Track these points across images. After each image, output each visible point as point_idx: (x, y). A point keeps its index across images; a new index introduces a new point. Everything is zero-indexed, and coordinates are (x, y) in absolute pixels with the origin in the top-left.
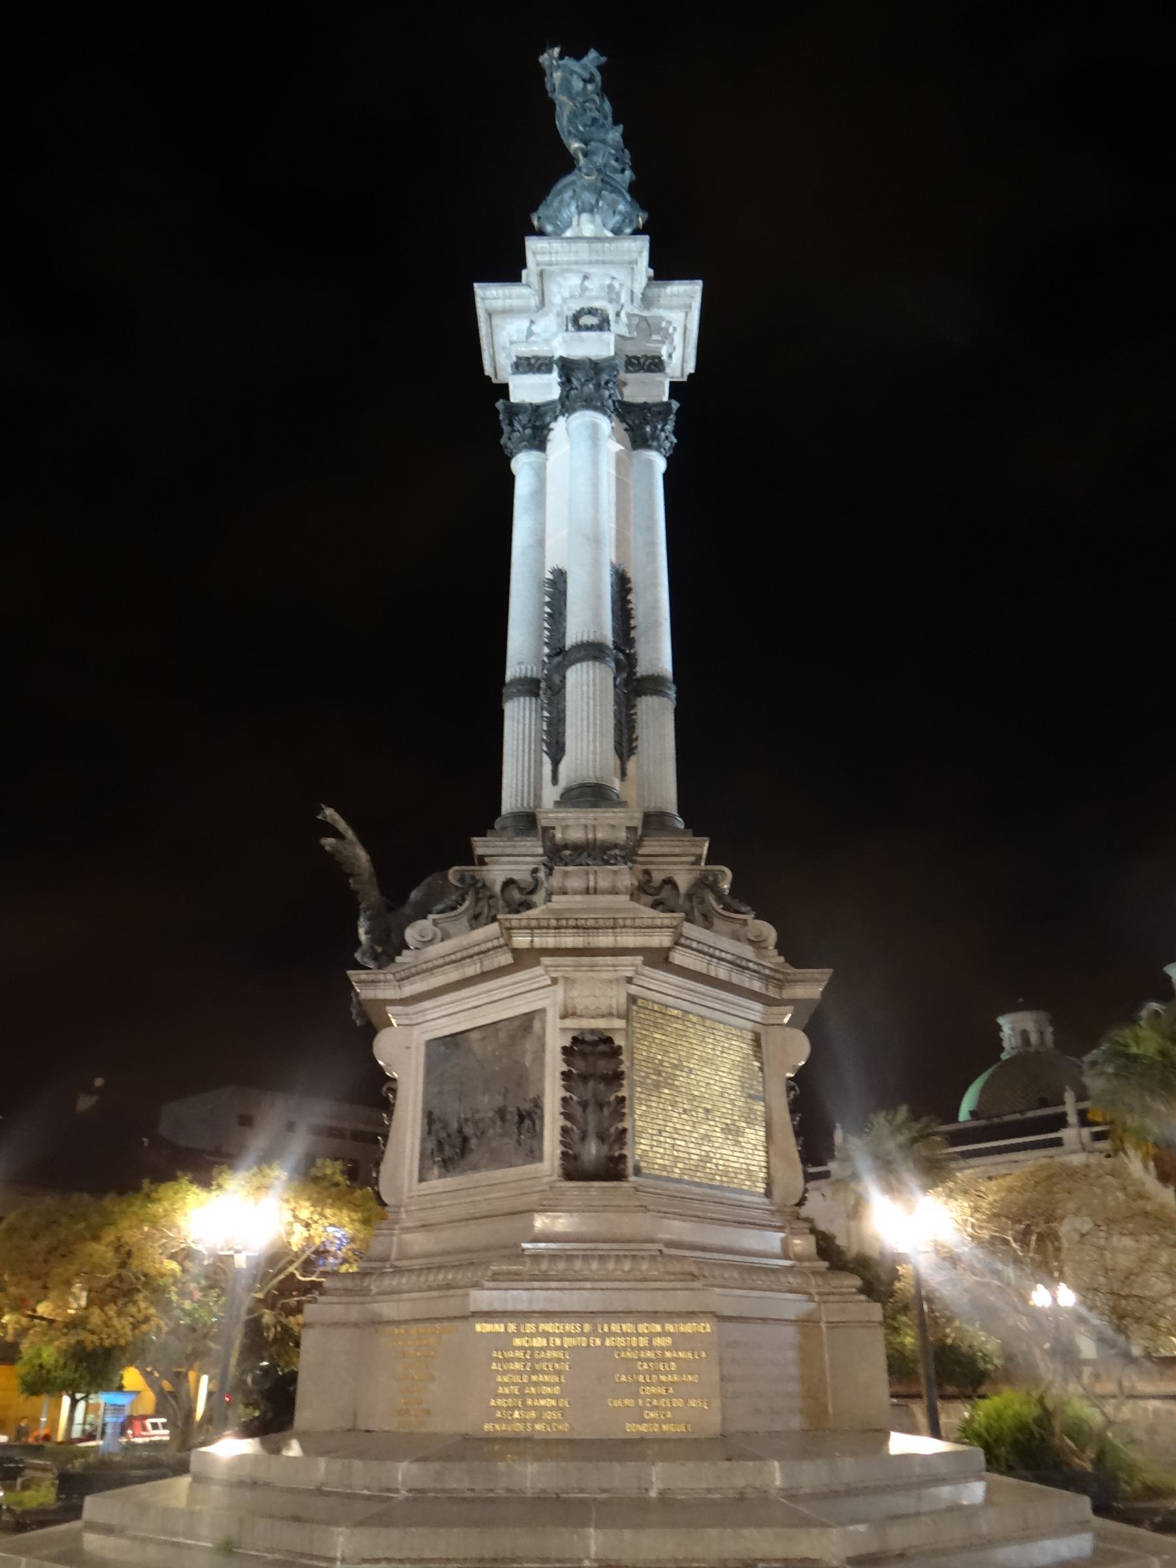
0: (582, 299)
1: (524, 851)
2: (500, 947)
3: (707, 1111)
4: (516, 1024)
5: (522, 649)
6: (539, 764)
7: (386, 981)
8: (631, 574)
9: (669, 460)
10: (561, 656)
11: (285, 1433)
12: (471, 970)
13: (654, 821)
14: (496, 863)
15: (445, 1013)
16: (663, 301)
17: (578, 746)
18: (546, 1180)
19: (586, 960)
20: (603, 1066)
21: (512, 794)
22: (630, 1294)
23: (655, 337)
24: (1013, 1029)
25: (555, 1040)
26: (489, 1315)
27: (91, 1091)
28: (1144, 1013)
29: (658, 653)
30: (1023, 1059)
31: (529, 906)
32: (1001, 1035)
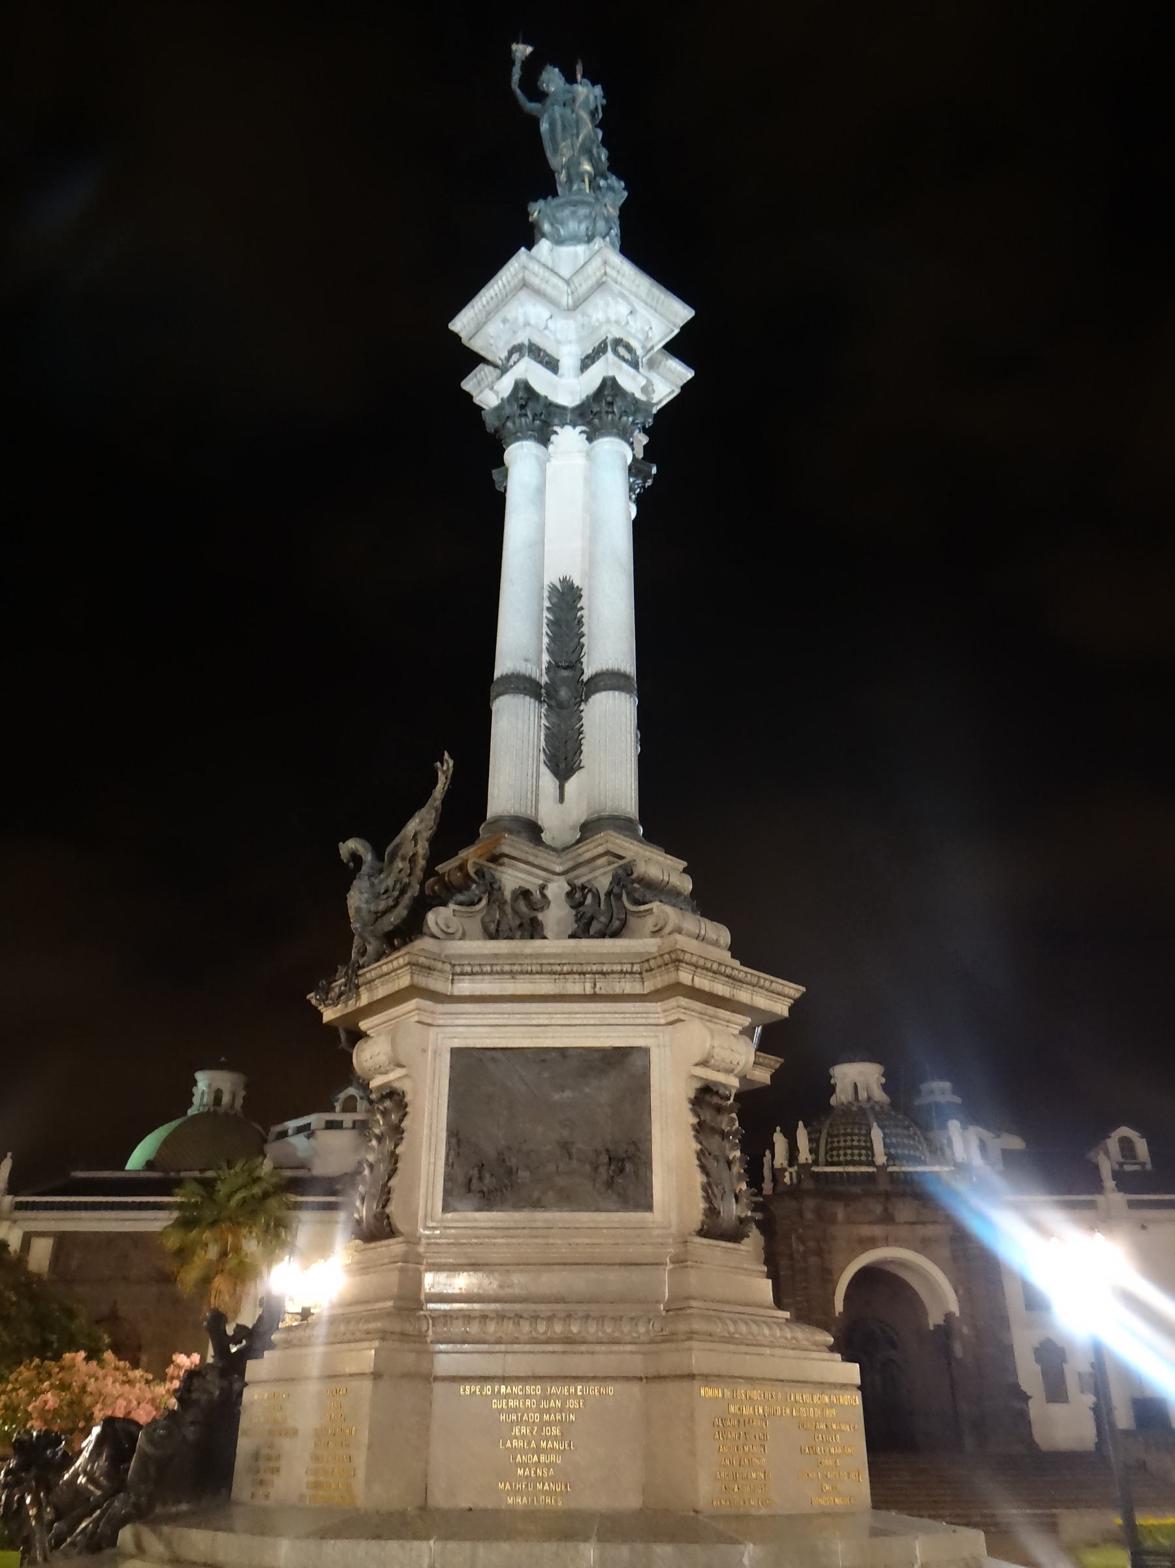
0: (574, 319)
1: (544, 863)
5: (519, 640)
7: (441, 971)
12: (545, 986)
14: (511, 866)
15: (493, 1022)
17: (566, 770)
19: (711, 1010)
24: (210, 1086)
28: (342, 1096)
29: (611, 639)
30: (215, 1115)
32: (194, 1090)
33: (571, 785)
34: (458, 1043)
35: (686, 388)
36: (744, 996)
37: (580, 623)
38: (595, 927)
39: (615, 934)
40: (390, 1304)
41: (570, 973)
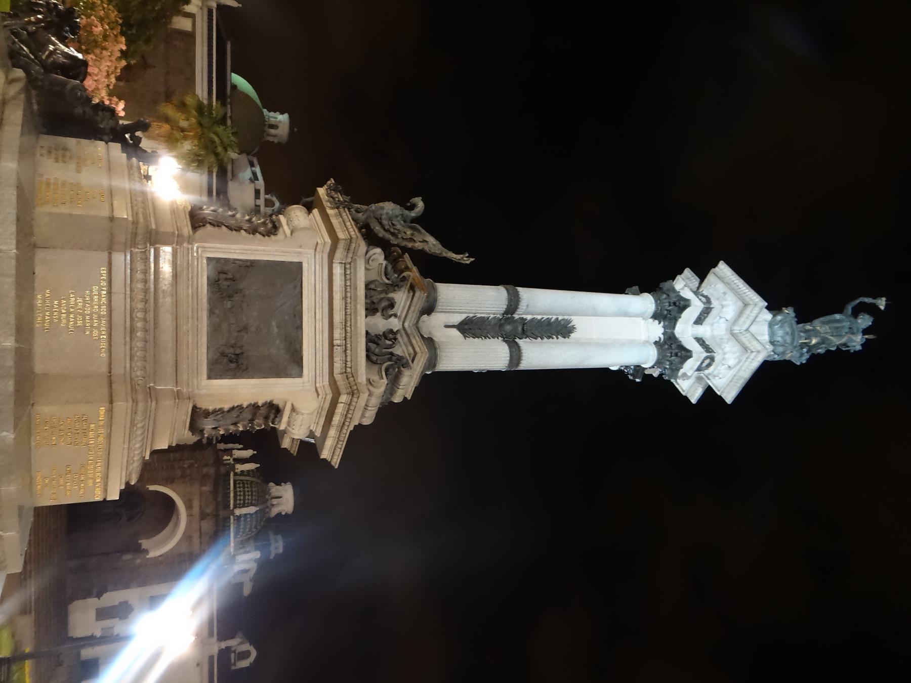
0: (725, 334)
1: (410, 316)
2: (346, 367)
4: (298, 347)
5: (540, 302)
7: (347, 256)
11: (28, 532)
14: (408, 297)
17: (464, 329)
18: (195, 381)
22: (122, 296)
24: (280, 122)
26: (110, 411)
28: (274, 199)
29: (540, 355)
30: (263, 125)
33: (455, 332)
34: (305, 266)
35: (720, 398)
36: (332, 432)
37: (549, 337)
38: (373, 346)
39: (368, 357)
40: (154, 227)
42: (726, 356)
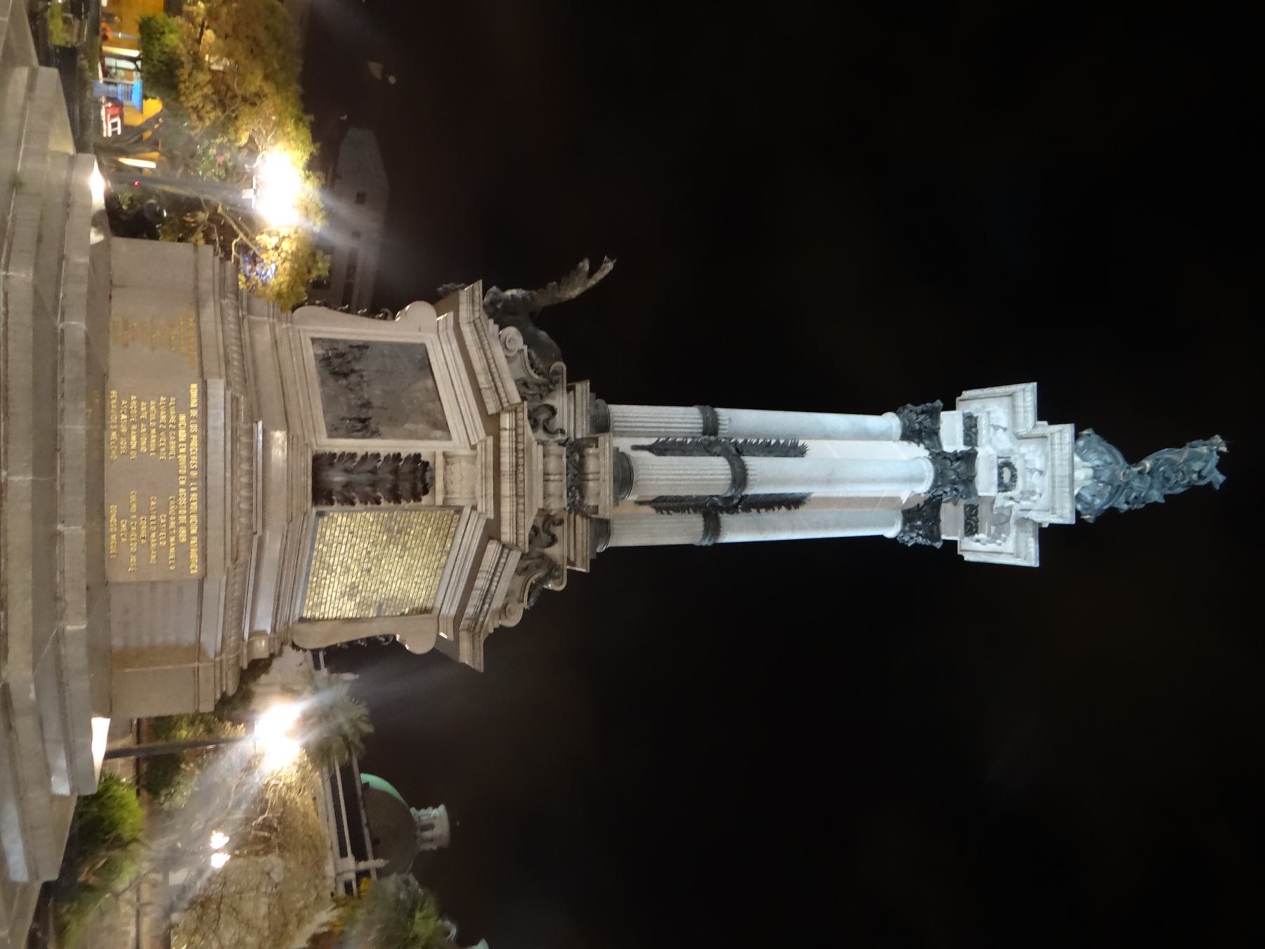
0: (1028, 469)
1: (579, 423)
3: (369, 571)
4: (439, 416)
5: (742, 421)
6: (649, 435)
7: (474, 311)
8: (802, 509)
9: (894, 540)
10: (736, 452)
13: (602, 528)
14: (569, 399)
16: (1022, 535)
17: (665, 468)
18: (313, 440)
20: (405, 487)
21: (620, 412)
23: (993, 528)
24: (435, 817)
25: (426, 448)
26: (204, 394)
27: (385, 74)
28: (448, 923)
29: (738, 531)
30: (411, 827)
31: (534, 426)
34: (429, 347)
41: (492, 374)
42: (1027, 457)
